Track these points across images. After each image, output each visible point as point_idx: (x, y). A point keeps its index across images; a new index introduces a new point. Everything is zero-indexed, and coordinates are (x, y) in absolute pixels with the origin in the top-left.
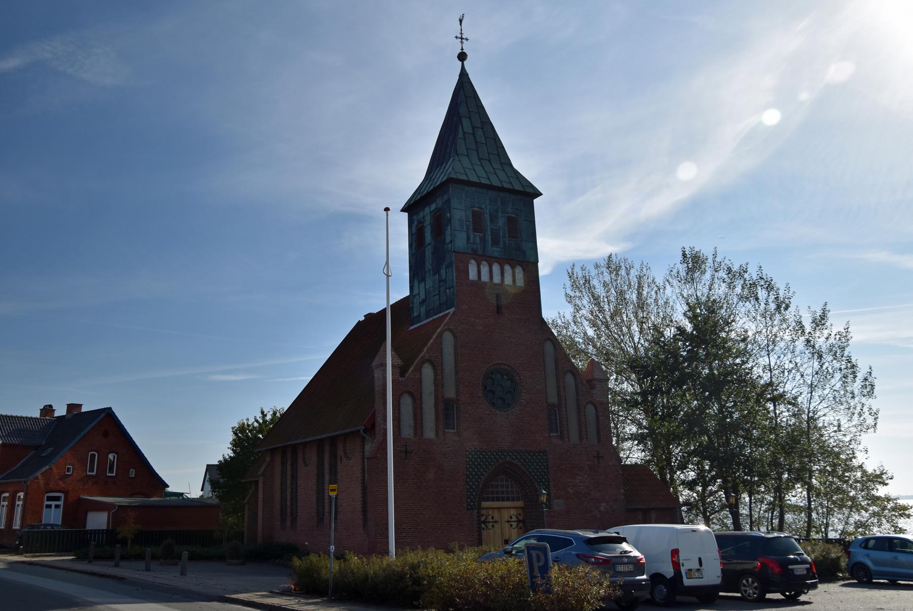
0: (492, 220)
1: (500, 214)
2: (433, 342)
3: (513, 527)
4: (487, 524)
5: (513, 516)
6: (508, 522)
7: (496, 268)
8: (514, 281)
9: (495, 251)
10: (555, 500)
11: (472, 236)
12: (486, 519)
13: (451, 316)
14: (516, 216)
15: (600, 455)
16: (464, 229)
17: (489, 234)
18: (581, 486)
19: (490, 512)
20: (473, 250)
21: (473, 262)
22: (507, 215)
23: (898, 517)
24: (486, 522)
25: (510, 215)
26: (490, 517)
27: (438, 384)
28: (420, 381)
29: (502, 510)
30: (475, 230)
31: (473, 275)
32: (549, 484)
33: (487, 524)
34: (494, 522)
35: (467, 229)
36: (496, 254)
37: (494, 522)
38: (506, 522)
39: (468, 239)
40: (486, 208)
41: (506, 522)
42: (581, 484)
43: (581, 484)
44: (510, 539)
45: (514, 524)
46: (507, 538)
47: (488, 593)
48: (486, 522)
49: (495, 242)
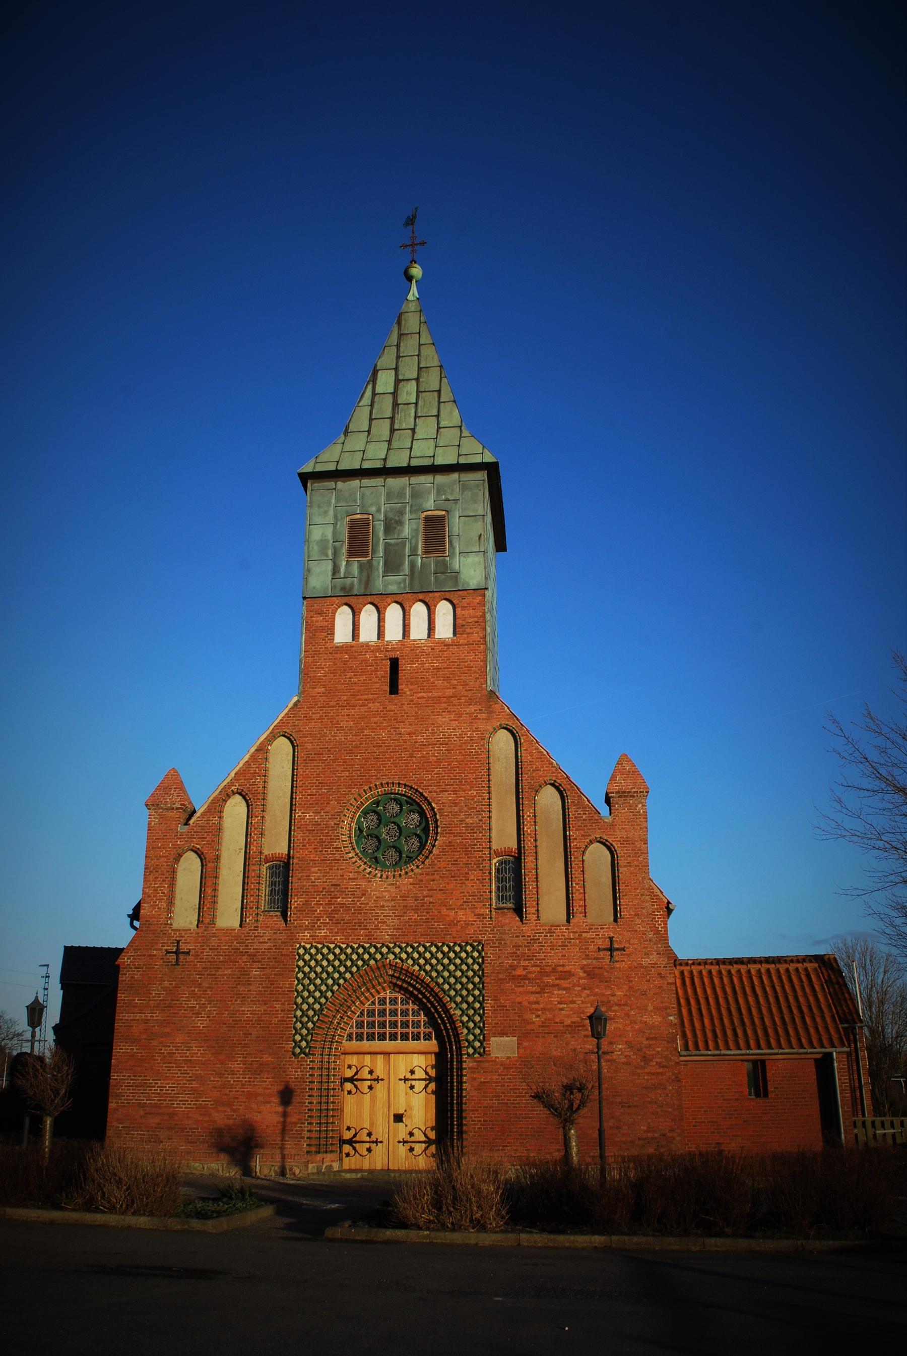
0: (388, 529)
1: (407, 516)
2: (249, 759)
3: (416, 1090)
4: (357, 1145)
5: (417, 1069)
6: (377, 1080)
7: (419, 611)
8: (381, 633)
9: (393, 583)
10: (493, 1039)
11: (344, 563)
12: (356, 1073)
13: (289, 711)
14: (444, 513)
15: (616, 946)
16: (327, 556)
17: (381, 555)
18: (562, 1009)
19: (367, 1059)
20: (343, 589)
21: (346, 610)
22: (423, 515)
23: (578, 1084)
24: (358, 1080)
25: (429, 513)
26: (367, 1070)
27: (253, 831)
28: (218, 830)
29: (392, 1056)
30: (351, 554)
31: (342, 634)
32: (482, 1007)
33: (357, 1145)
34: (374, 1080)
35: (336, 553)
36: (393, 588)
37: (374, 1080)
38: (401, 1080)
39: (335, 570)
40: (379, 511)
41: (401, 1080)
42: (562, 1006)
43: (562, 1006)
44: (408, 1113)
45: (419, 1085)
46: (401, 1112)
47: (40, 1204)
48: (358, 1080)
49: (391, 566)
